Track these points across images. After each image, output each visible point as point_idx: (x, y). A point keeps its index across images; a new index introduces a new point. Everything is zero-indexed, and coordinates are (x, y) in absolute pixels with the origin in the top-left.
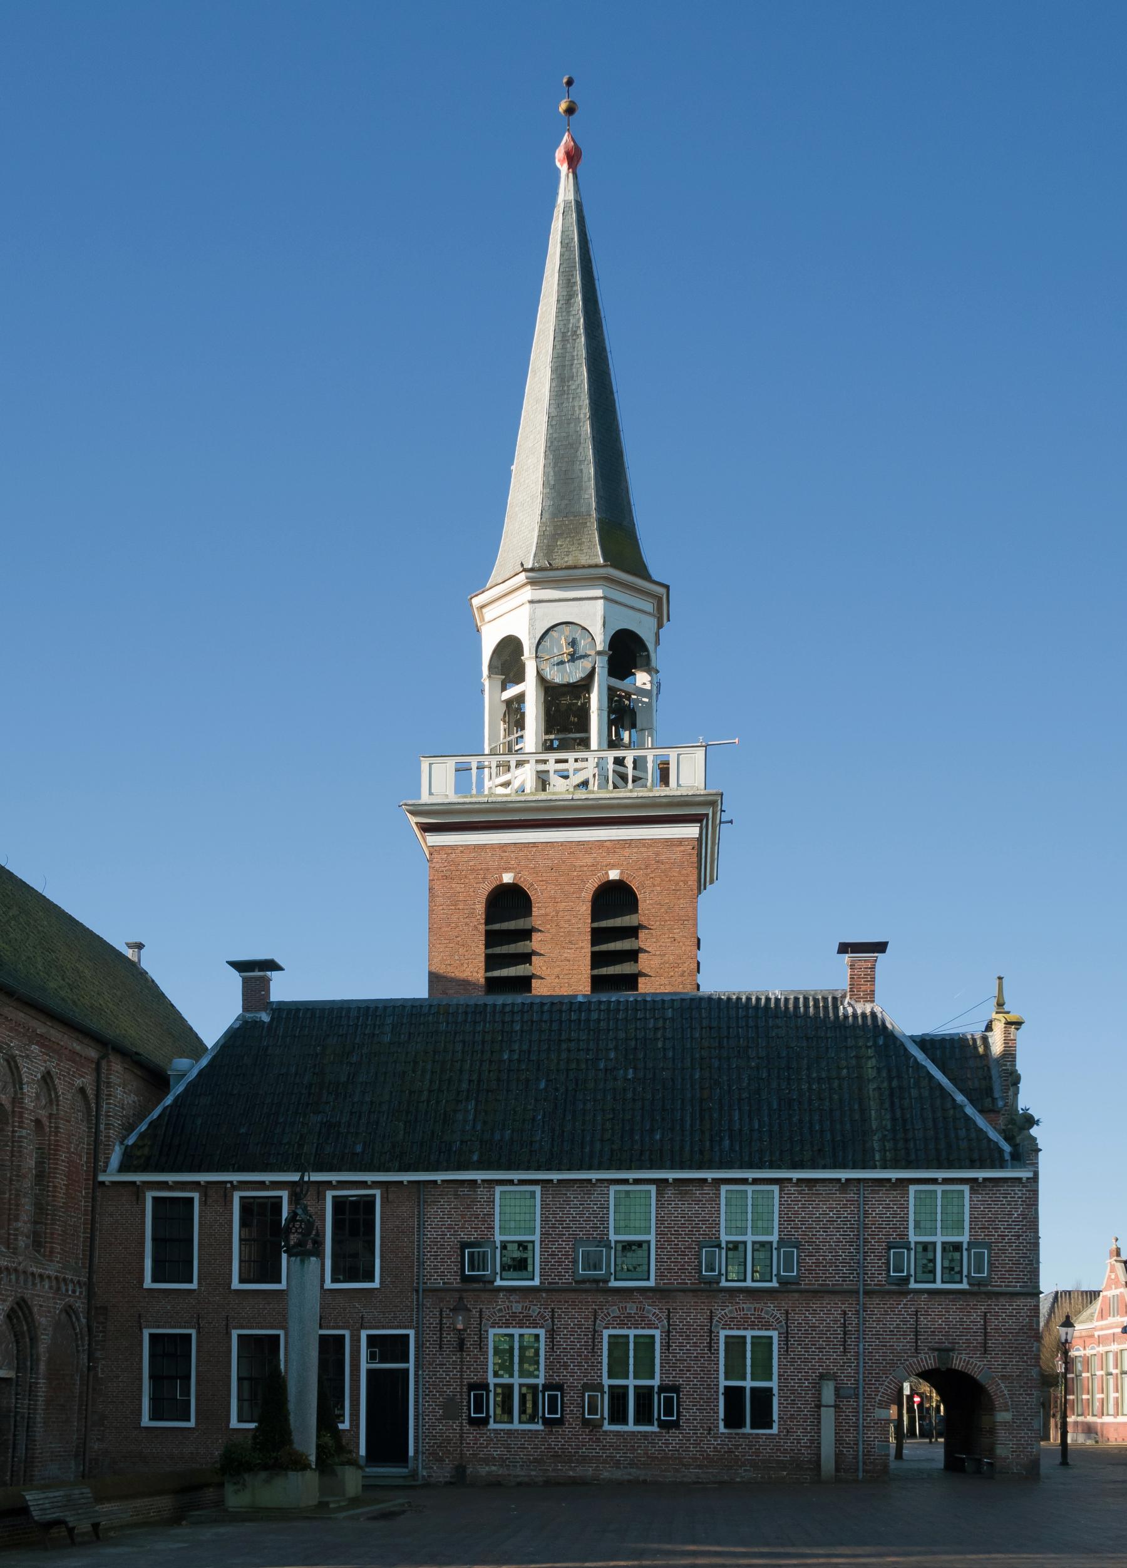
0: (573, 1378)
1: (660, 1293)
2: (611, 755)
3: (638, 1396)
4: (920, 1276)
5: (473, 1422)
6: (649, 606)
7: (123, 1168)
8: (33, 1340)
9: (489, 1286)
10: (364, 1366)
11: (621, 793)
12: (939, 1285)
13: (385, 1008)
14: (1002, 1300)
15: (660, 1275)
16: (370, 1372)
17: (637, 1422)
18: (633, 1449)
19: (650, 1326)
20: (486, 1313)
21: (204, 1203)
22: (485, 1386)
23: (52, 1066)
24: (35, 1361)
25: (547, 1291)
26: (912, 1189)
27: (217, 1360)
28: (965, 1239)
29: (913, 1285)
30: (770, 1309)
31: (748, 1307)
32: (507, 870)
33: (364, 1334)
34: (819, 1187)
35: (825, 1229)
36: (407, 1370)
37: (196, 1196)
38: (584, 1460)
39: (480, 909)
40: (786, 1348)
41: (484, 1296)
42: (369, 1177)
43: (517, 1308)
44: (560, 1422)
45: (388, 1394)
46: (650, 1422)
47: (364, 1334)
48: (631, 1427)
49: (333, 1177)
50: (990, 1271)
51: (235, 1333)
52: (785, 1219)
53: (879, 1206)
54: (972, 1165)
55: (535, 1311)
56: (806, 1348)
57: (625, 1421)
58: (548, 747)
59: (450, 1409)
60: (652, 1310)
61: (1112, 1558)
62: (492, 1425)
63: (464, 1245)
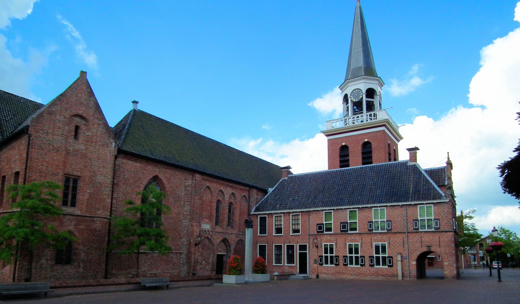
2: (368, 114)
5: (320, 264)
6: (377, 82)
7: (255, 211)
8: (230, 246)
12: (426, 230)
13: (439, 171)
14: (443, 233)
16: (300, 253)
17: (383, 265)
18: (355, 271)
19: (384, 241)
22: (322, 256)
23: (233, 191)
24: (230, 251)
25: (335, 234)
28: (433, 218)
29: (420, 230)
30: (385, 237)
31: (380, 237)
34: (396, 207)
38: (344, 274)
42: (298, 210)
43: (328, 238)
44: (338, 265)
46: (386, 265)
47: (298, 245)
49: (291, 211)
52: (388, 215)
53: (410, 210)
54: (434, 199)
55: (332, 239)
57: (352, 264)
59: (315, 262)
60: (357, 238)
61: (103, 292)
62: (375, 266)
63: (317, 224)
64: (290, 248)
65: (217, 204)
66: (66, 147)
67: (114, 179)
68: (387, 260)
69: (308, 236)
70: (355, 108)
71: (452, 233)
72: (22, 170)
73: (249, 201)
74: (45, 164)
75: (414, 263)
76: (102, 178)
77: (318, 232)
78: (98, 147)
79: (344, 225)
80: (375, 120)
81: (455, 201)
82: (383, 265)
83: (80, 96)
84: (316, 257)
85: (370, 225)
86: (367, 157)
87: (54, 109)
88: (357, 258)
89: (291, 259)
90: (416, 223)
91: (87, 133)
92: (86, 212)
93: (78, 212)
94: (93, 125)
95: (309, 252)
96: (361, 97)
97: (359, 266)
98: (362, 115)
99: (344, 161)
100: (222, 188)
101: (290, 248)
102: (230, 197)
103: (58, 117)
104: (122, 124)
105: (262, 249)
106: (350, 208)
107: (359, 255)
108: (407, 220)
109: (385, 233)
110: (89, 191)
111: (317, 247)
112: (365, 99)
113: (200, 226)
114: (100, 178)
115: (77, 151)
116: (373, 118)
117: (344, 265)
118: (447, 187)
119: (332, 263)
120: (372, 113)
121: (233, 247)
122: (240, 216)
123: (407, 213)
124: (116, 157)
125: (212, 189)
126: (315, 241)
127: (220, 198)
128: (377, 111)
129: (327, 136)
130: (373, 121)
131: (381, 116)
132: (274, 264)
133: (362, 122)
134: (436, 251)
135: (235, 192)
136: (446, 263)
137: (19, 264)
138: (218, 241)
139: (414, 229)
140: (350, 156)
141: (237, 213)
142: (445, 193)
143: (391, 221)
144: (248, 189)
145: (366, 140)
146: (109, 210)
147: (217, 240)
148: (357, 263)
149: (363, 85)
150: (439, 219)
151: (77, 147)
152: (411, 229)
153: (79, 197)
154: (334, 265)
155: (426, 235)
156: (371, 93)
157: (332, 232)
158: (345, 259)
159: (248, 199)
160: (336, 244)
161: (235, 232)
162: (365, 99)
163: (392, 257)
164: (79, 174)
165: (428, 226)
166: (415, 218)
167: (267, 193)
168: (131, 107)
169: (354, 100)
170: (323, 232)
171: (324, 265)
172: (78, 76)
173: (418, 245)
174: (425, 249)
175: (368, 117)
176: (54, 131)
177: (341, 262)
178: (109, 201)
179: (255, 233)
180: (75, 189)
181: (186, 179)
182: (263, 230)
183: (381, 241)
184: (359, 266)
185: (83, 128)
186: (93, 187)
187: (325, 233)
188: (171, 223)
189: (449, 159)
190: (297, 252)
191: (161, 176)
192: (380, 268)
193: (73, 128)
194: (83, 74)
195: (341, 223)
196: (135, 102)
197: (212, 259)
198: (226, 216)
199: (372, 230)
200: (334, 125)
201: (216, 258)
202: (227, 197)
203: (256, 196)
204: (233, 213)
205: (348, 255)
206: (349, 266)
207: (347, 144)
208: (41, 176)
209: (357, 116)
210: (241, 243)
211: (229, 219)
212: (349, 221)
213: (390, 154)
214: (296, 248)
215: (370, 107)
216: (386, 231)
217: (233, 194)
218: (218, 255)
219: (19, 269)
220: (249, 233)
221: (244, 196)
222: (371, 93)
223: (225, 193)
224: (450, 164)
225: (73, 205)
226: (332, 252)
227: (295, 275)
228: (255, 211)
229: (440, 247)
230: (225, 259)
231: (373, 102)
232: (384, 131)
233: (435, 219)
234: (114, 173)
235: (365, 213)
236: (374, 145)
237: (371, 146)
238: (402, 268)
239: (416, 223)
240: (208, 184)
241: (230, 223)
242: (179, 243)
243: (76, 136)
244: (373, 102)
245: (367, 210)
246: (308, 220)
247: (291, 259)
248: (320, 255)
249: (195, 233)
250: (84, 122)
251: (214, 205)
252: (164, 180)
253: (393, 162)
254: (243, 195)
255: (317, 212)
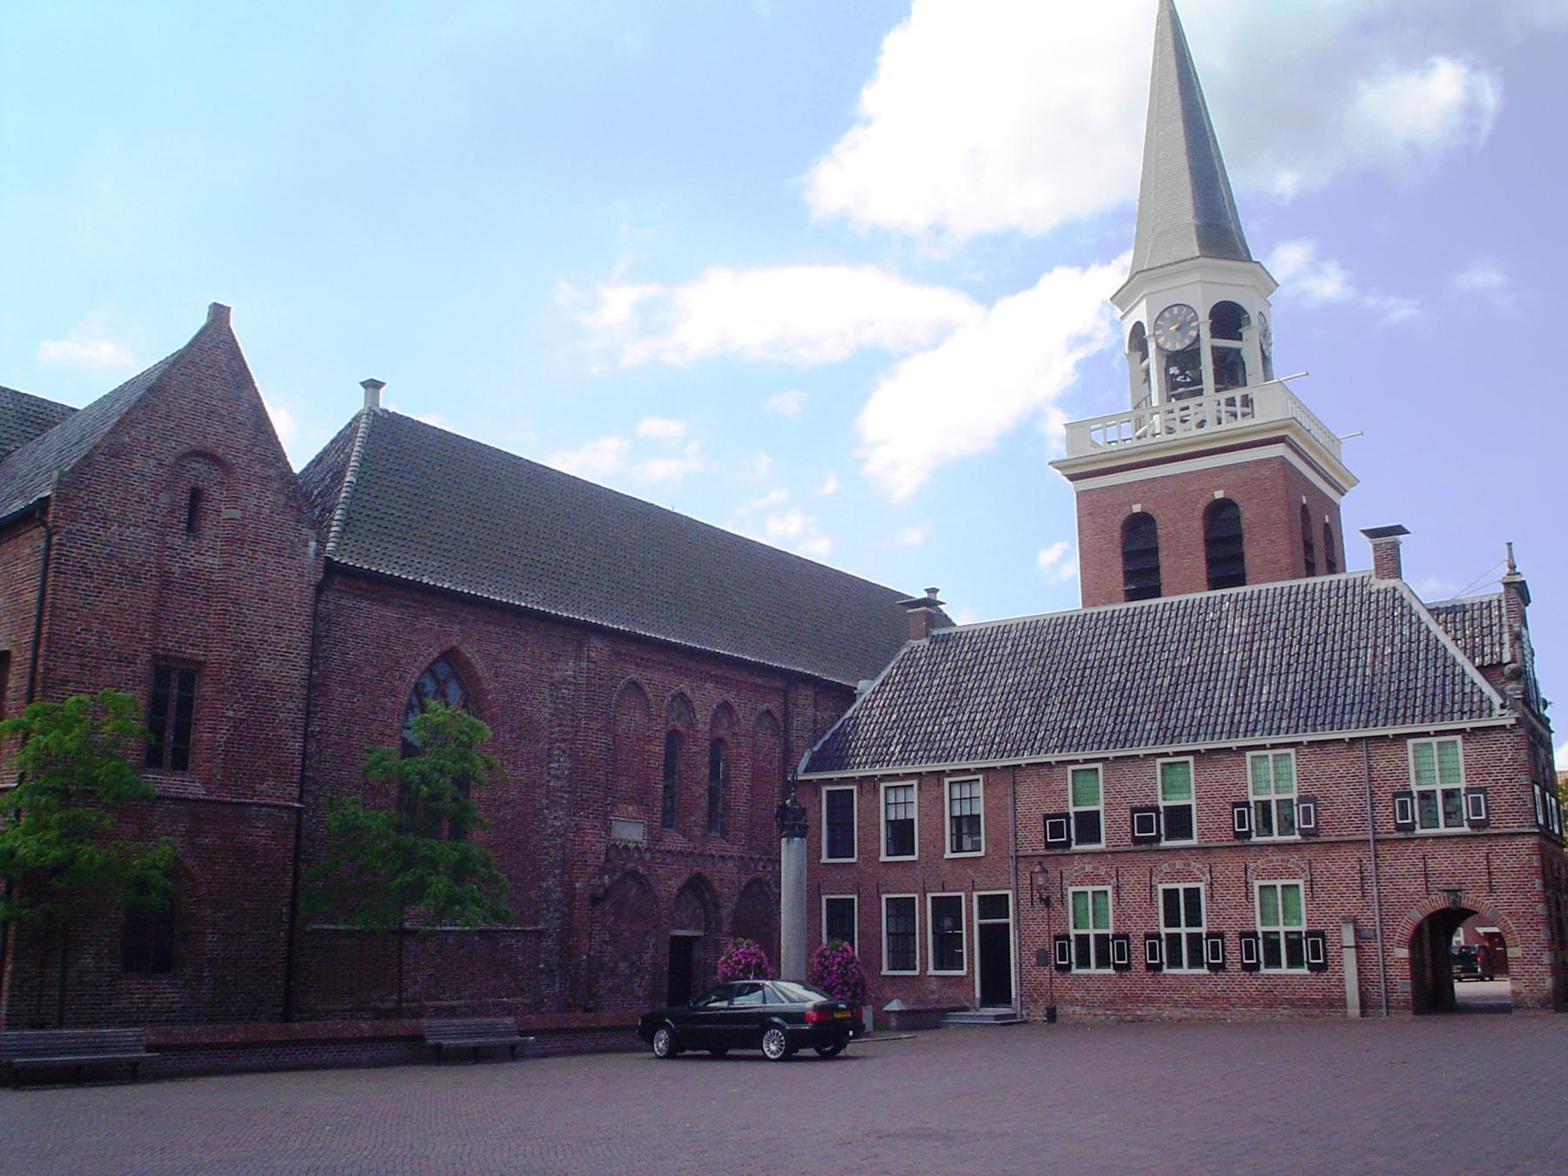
0: (1137, 930)
1: (1203, 850)
3: (1288, 941)
4: (1426, 823)
5: (1058, 967)
7: (806, 771)
8: (716, 906)
9: (1246, 842)
10: (976, 921)
11: (1220, 428)
14: (1502, 841)
15: (1202, 835)
16: (981, 926)
17: (1191, 966)
19: (1294, 875)
20: (1066, 874)
21: (860, 793)
22: (1067, 937)
26: (1410, 742)
27: (872, 919)
29: (1419, 831)
30: (1294, 859)
31: (1277, 858)
32: (1137, 502)
33: (975, 895)
34: (1330, 748)
35: (1337, 785)
36: (1008, 925)
37: (855, 788)
38: (1150, 1000)
39: (1117, 535)
40: (1312, 895)
41: (1063, 859)
43: (1088, 868)
44: (1128, 967)
45: (995, 942)
46: (1301, 964)
48: (1284, 970)
50: (1487, 814)
51: (884, 897)
52: (1303, 778)
53: (1383, 761)
55: (1102, 870)
56: (1329, 894)
58: (1217, 391)
59: (1042, 958)
62: (1264, 971)
63: (1047, 817)
64: (947, 909)
65: (667, 746)
66: (159, 566)
67: (312, 666)
68: (1112, 948)
69: (1012, 863)
70: (1174, 370)
71: (1532, 840)
72: (18, 645)
73: (786, 732)
74: (96, 626)
75: (1403, 952)
76: (273, 666)
77: (1048, 846)
78: (261, 556)
79: (1143, 817)
80: (1248, 422)
81: (1545, 722)
82: (1291, 964)
83: (205, 382)
84: (1044, 941)
85: (1241, 814)
86: (1225, 564)
87: (127, 439)
88: (1195, 940)
89: (948, 952)
90: (1403, 805)
91: (227, 513)
92: (223, 786)
93: (197, 790)
94: (248, 482)
95: (1018, 921)
96: (1194, 334)
97: (1205, 971)
98: (1198, 400)
99: (1142, 576)
100: (684, 686)
101: (947, 909)
102: (715, 718)
103: (138, 464)
104: (329, 462)
105: (840, 914)
106: (1166, 755)
107: (1203, 930)
108: (1372, 793)
109: (1295, 844)
110: (231, 713)
111: (1047, 902)
112: (1207, 344)
113: (608, 829)
114: (266, 667)
115: (195, 574)
116: (1239, 409)
117: (1149, 967)
118: (1506, 670)
119: (1103, 961)
120: (1237, 393)
121: (728, 908)
122: (752, 788)
123: (1370, 768)
124: (320, 589)
125: (647, 690)
126: (1040, 881)
127: (680, 726)
128: (1254, 386)
129: (1072, 478)
130: (1241, 423)
131: (1269, 409)
132: (885, 972)
133: (1201, 424)
134: (1477, 907)
135: (730, 697)
136: (1514, 952)
137: (13, 972)
138: (675, 884)
139: (1399, 828)
140: (1162, 555)
141: (742, 780)
142: (1502, 693)
143: (1314, 800)
144: (778, 684)
145: (1219, 494)
146: (296, 778)
147: (670, 883)
148: (1196, 961)
149: (1200, 293)
150: (1483, 790)
151: (194, 562)
152: (1387, 828)
153: (201, 734)
154: (1111, 971)
155: (1442, 850)
156: (1228, 319)
157: (1102, 846)
158: (1152, 946)
159: (781, 725)
160: (1117, 889)
161: (735, 851)
162: (1207, 344)
163: (1321, 934)
164: (199, 654)
165: (1447, 815)
166: (1398, 788)
167: (853, 699)
168: (356, 403)
169: (1168, 346)
170: (1067, 844)
171: (1075, 971)
172: (202, 320)
173: (1415, 886)
174: (1439, 902)
175: (1223, 407)
176: (124, 513)
177: (1139, 956)
178: (297, 745)
179: (813, 853)
180: (186, 706)
181: (555, 658)
182: (841, 843)
183: (1281, 875)
184: (1205, 971)
185: (216, 493)
186: (245, 697)
187: (1075, 847)
188: (505, 822)
189: (1512, 567)
190: (972, 923)
191: (469, 652)
192: (1281, 977)
193: (184, 499)
194: (219, 314)
195: (1134, 810)
196: (373, 386)
197: (654, 954)
198: (701, 790)
199: (1248, 835)
200: (1098, 436)
201: (667, 949)
202: (703, 718)
203: (810, 712)
204: (727, 780)
205: (1164, 931)
206: (1166, 970)
207: (1151, 509)
208: (82, 666)
209: (1184, 403)
210: (762, 894)
211: (713, 802)
212: (1162, 804)
213: (1308, 547)
214: (969, 908)
215: (1230, 370)
216: (1297, 837)
217: (725, 707)
218: (674, 938)
219: (11, 987)
220: (791, 855)
221: (768, 712)
222: (1228, 319)
223: (696, 704)
224: (1518, 591)
225: (181, 763)
226: (1194, 920)
227: (965, 1009)
228: (806, 771)
229: (1491, 889)
230: (698, 954)
231: (1238, 351)
232: (1283, 460)
233: (1469, 790)
234: (313, 649)
235: (1219, 772)
236: (1247, 515)
237: (1239, 518)
238: (1360, 972)
239: (1403, 805)
240: (634, 674)
241: (716, 818)
242: (532, 893)
243: (192, 526)
244: (1238, 351)
245: (1228, 760)
246: (1010, 800)
247: (948, 952)
248: (1059, 931)
249: (590, 858)
250: (217, 474)
251: (658, 748)
252: (480, 667)
253: (1327, 578)
254: (765, 707)
255: (1045, 770)
